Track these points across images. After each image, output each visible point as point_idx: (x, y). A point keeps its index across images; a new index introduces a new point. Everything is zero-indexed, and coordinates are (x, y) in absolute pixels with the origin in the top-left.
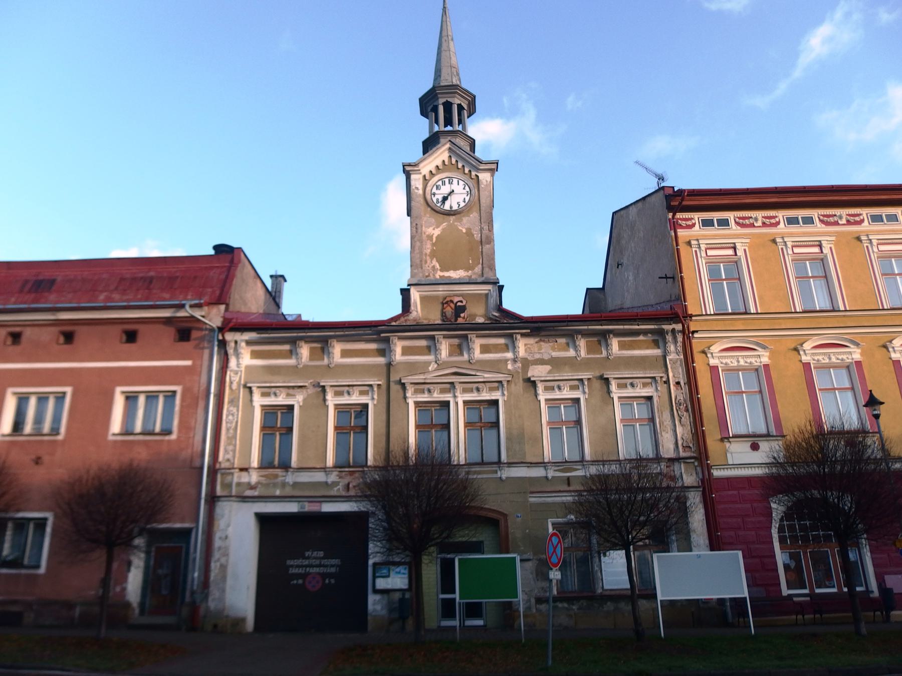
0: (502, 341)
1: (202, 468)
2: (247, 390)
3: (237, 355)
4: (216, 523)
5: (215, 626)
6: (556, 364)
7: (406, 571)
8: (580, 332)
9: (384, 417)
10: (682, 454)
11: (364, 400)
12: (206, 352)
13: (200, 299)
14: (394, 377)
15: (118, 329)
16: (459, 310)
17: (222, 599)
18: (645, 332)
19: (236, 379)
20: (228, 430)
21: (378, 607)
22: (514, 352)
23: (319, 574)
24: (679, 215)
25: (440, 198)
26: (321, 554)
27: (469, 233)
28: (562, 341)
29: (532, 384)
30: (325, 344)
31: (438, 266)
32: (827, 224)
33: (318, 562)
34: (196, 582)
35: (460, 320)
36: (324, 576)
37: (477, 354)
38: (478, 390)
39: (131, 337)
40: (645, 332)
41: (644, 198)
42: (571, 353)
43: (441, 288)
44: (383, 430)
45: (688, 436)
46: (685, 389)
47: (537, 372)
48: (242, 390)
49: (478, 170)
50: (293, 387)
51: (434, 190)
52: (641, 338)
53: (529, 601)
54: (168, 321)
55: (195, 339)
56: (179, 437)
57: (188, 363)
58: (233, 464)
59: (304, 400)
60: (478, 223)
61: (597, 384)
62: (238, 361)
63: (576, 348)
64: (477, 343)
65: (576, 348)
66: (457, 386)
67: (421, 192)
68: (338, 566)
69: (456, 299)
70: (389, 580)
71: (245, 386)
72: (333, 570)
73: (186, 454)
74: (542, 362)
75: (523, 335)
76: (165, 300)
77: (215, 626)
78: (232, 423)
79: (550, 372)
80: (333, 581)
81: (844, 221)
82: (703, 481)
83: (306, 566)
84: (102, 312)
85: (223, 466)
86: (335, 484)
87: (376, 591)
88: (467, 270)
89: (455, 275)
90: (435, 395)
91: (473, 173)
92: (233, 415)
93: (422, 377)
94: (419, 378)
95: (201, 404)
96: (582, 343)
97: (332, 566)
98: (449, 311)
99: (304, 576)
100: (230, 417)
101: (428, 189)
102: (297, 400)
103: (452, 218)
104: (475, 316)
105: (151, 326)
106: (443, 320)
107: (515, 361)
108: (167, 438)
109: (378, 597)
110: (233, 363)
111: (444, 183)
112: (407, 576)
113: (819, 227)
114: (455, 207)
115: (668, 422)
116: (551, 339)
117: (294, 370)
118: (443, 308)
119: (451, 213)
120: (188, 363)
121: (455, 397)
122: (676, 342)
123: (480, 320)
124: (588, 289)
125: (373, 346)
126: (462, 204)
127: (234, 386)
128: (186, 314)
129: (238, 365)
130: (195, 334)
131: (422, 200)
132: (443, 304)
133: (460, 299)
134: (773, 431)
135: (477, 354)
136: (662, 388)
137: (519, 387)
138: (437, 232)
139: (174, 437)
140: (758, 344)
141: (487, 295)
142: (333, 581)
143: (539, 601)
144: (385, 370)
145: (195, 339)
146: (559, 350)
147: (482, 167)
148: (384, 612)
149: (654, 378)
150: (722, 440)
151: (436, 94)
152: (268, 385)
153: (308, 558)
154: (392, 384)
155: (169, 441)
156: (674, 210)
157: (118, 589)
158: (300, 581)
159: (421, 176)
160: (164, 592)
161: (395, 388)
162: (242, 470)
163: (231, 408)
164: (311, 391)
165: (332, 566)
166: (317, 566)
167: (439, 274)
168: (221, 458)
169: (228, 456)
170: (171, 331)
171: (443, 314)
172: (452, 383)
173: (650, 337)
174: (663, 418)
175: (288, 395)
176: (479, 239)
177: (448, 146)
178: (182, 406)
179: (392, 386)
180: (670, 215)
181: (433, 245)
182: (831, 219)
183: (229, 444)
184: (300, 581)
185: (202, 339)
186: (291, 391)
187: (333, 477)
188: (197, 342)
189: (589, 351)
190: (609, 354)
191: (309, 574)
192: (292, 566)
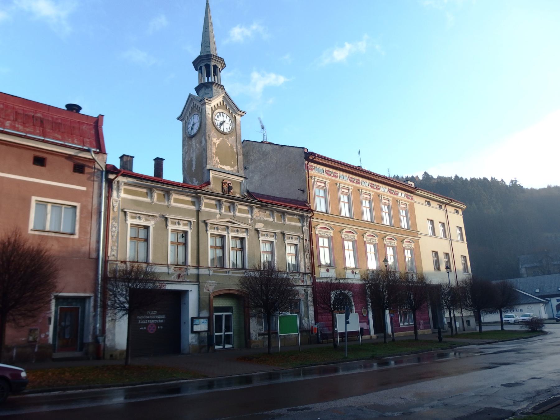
0: (246, 208)
1: (97, 259)
2: (123, 213)
3: (118, 190)
4: (549, 294)
5: (111, 356)
6: (266, 223)
7: (207, 322)
8: (276, 210)
9: (196, 239)
10: (307, 271)
11: (186, 228)
12: (96, 184)
13: (84, 146)
14: (202, 218)
15: (30, 156)
16: (230, 188)
17: (113, 340)
18: (297, 215)
19: (116, 205)
20: (112, 236)
21: (194, 341)
22: (252, 215)
23: (154, 323)
24: (310, 164)
25: (219, 123)
26: (155, 312)
27: (231, 147)
28: (268, 212)
29: (257, 231)
30: (167, 194)
31: (219, 161)
32: (328, 174)
33: (154, 317)
34: (98, 331)
35: (230, 194)
36: (157, 325)
37: (173, 203)
38: (238, 231)
39: (39, 161)
40: (297, 215)
41: (282, 146)
42: (271, 219)
43: (223, 174)
44: (196, 247)
45: (309, 264)
46: (309, 243)
47: (259, 226)
48: (120, 212)
49: (236, 113)
50: (149, 215)
51: (216, 117)
52: (295, 217)
53: (256, 335)
54: (69, 157)
55: (88, 173)
56: (80, 237)
57: (84, 189)
58: (117, 258)
59: (155, 224)
60: (235, 143)
61: (280, 236)
62: (118, 194)
63: (273, 217)
64: (174, 196)
65: (152, 197)
66: (230, 228)
67: (210, 116)
68: (164, 319)
69: (228, 182)
70: (199, 326)
71: (122, 210)
72: (162, 321)
73: (85, 249)
74: (260, 222)
75: (257, 207)
76: (18, 131)
77: (111, 356)
78: (115, 232)
79: (263, 227)
80: (162, 327)
81: (332, 175)
82: (313, 283)
83: (148, 319)
84: (85, 153)
85: (110, 259)
86: (173, 274)
87: (193, 332)
88: (231, 167)
89: (227, 168)
90: (220, 231)
91: (234, 114)
92: (115, 227)
93: (215, 221)
94: (214, 221)
95: (95, 218)
96: (276, 214)
97: (161, 319)
98: (225, 187)
99: (147, 325)
100: (114, 229)
101: (214, 116)
102: (151, 224)
103: (224, 136)
104: (236, 193)
105: (57, 158)
106: (223, 192)
107: (252, 219)
108: (72, 237)
109: (193, 335)
110: (115, 194)
111: (220, 115)
112: (207, 324)
113: (325, 175)
114: (225, 131)
115: (302, 257)
116: (264, 211)
117: (149, 206)
118: (223, 186)
119: (223, 133)
120: (84, 189)
121: (228, 233)
122: (307, 221)
123: (238, 195)
124: (132, 157)
125: (189, 199)
126: (229, 130)
127: (115, 209)
128: (91, 157)
129: (118, 196)
130: (87, 170)
131: (210, 120)
132: (222, 183)
133: (230, 182)
134: (333, 265)
135: (173, 203)
136: (301, 241)
137: (253, 233)
138: (218, 142)
139: (76, 237)
140: (331, 227)
141: (240, 183)
142: (162, 327)
143: (259, 335)
144: (195, 213)
145: (88, 173)
146: (267, 217)
147: (239, 113)
148: (196, 343)
149: (190, 221)
150: (318, 266)
151: (211, 59)
152: (140, 212)
153: (149, 315)
154: (200, 222)
155: (73, 239)
156: (309, 161)
157: (43, 336)
158: (145, 328)
159: (210, 107)
160: (67, 337)
161: (202, 225)
162: (122, 262)
163: (114, 223)
164: (159, 219)
165: (161, 319)
166: (153, 319)
167: (219, 166)
168: (109, 254)
169: (113, 253)
170: (70, 165)
171: (223, 188)
172: (227, 227)
173: (298, 217)
174: (301, 255)
175: (146, 220)
176: (236, 151)
177: (223, 95)
178: (81, 217)
179: (200, 224)
180: (306, 162)
181: (216, 149)
182: (329, 173)
183: (114, 245)
184: (145, 328)
185: (93, 174)
186: (147, 217)
187: (171, 271)
188: (89, 176)
189: (158, 200)
190: (284, 223)
191: (149, 323)
192: (140, 319)
